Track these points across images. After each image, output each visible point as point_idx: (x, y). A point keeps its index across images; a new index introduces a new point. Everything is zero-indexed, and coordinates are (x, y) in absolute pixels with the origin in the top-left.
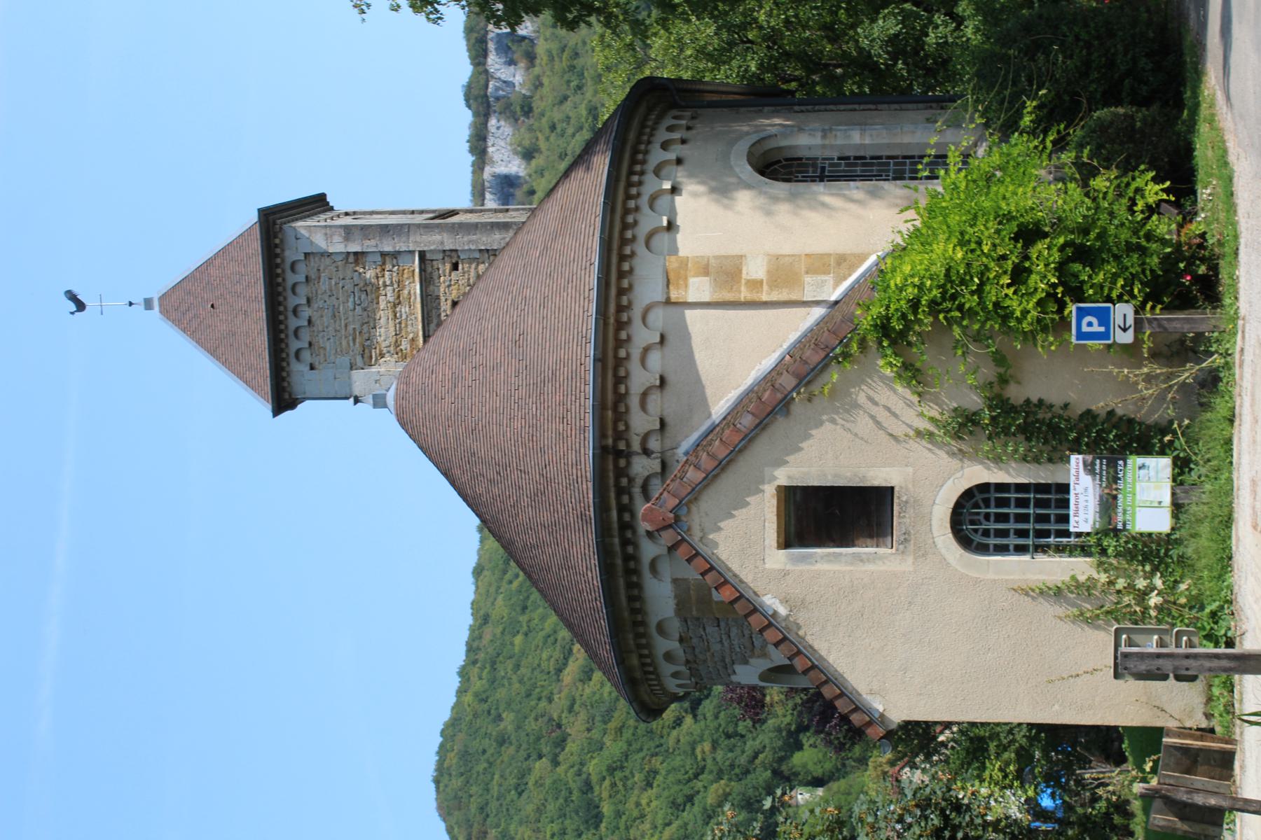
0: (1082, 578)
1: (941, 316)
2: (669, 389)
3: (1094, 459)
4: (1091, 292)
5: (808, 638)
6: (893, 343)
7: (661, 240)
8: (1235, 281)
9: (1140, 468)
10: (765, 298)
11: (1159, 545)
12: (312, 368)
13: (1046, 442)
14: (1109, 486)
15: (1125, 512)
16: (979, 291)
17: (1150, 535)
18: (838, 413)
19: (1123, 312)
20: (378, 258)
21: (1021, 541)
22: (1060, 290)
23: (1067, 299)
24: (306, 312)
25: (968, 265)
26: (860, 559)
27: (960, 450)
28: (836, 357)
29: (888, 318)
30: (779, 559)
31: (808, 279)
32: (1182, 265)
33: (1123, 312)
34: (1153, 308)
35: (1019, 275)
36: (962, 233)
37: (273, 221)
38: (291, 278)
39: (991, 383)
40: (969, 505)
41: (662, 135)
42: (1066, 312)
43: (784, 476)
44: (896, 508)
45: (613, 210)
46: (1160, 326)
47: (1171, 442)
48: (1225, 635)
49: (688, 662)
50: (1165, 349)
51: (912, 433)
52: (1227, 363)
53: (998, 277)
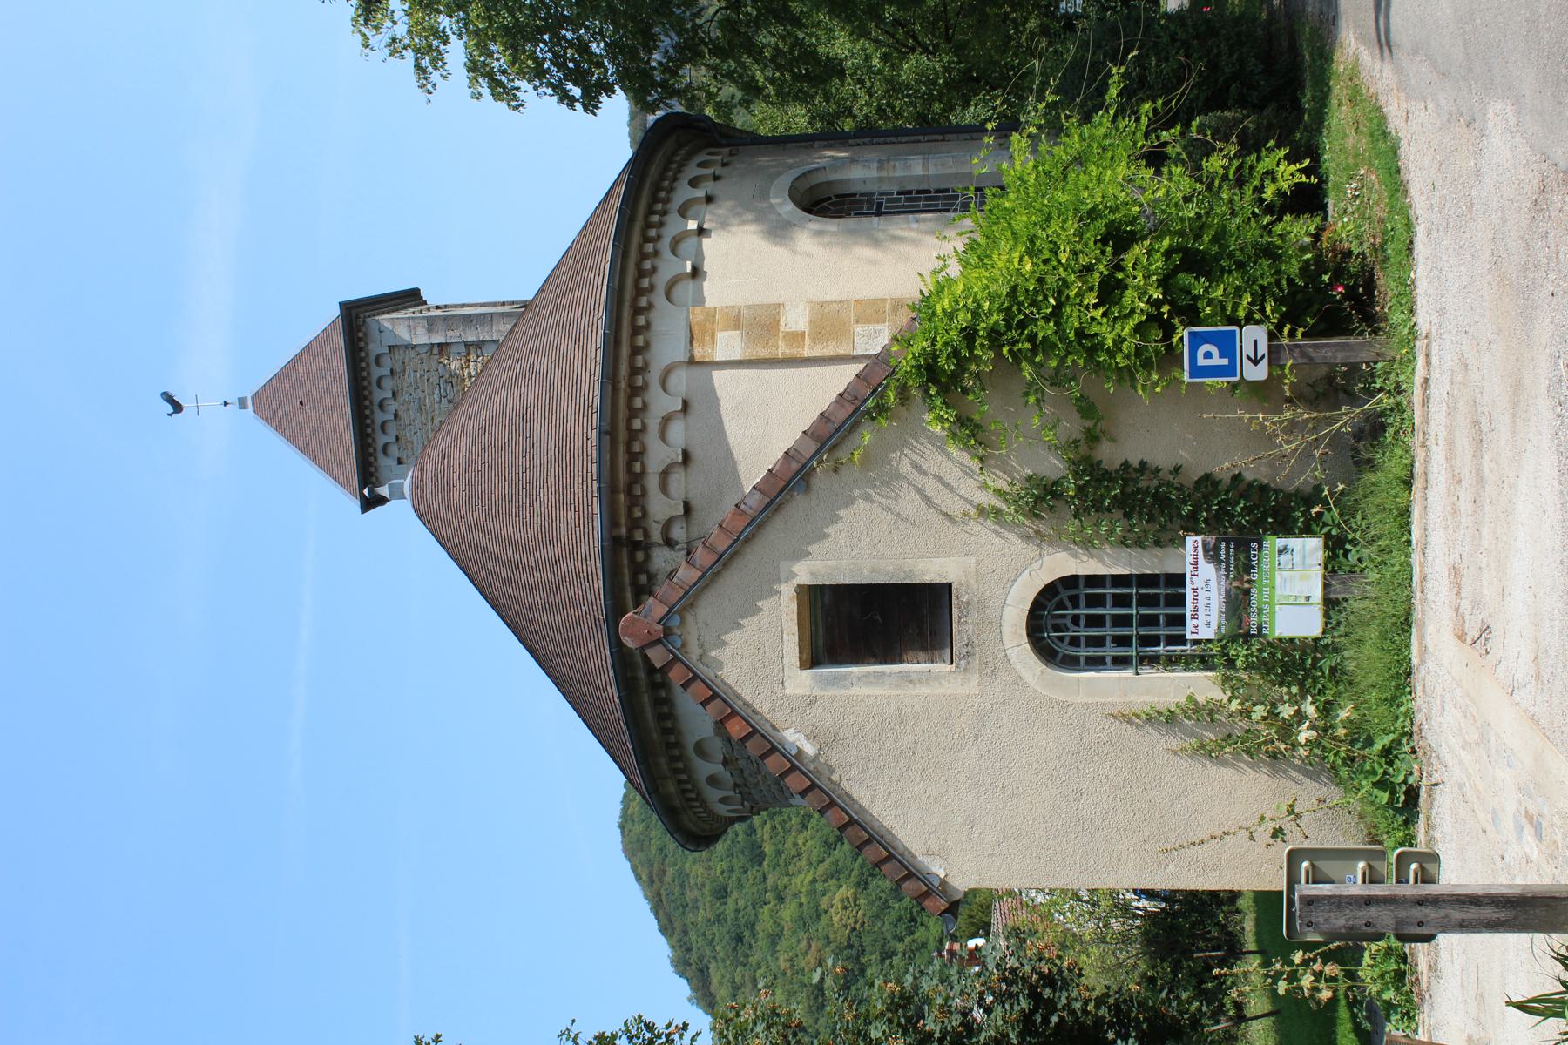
0: (1201, 700)
1: (1005, 350)
2: (694, 467)
3: (1218, 541)
4: (1208, 310)
5: (844, 784)
6: (944, 390)
7: (685, 290)
8: (1407, 289)
9: (1280, 552)
10: (807, 353)
11: (1304, 653)
12: (400, 462)
13: (1151, 519)
14: (1238, 578)
15: (1260, 611)
16: (1057, 313)
17: (1292, 640)
18: (873, 487)
19: (1254, 336)
20: (463, 349)
21: (1121, 652)
22: (1165, 309)
23: (1176, 321)
24: (392, 406)
25: (1041, 280)
26: (907, 678)
27: (1037, 532)
28: (868, 412)
29: (935, 356)
30: (802, 682)
31: (858, 329)
32: (1326, 278)
33: (1254, 336)
34: (1292, 334)
35: (1110, 291)
36: (1032, 240)
37: (356, 315)
38: (376, 372)
39: (1076, 442)
40: (1051, 604)
41: (692, 171)
42: (1175, 340)
43: (806, 572)
44: (955, 612)
45: (625, 255)
46: (1304, 355)
47: (1320, 515)
48: (1405, 782)
49: (736, 785)
50: (1307, 391)
51: (973, 511)
52: (1398, 404)
53: (1080, 295)
